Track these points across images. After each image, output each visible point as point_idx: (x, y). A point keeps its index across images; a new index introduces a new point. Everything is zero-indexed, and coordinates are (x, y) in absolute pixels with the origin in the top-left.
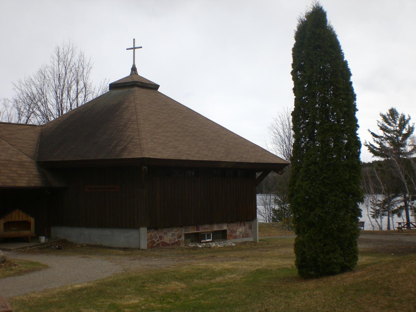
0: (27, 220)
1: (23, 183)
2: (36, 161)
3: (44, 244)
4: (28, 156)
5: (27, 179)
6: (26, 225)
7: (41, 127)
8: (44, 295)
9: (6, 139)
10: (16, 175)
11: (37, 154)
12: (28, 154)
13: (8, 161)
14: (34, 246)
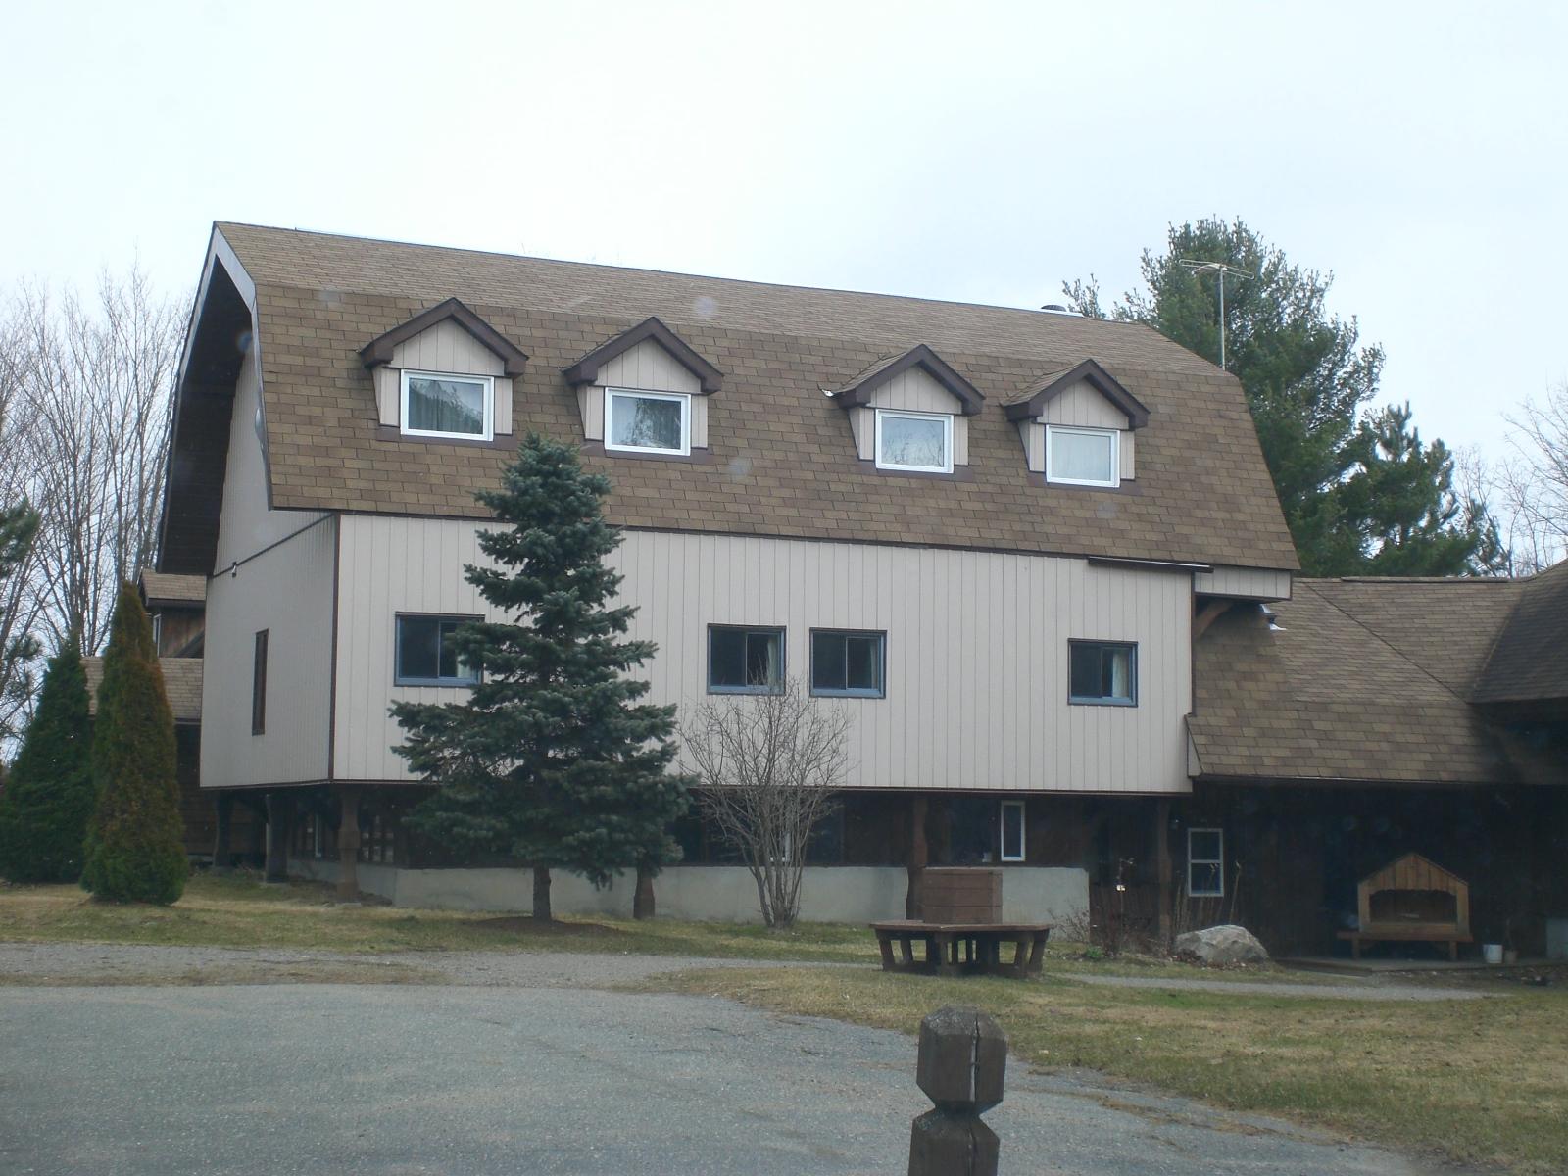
0: (1445, 889)
1: (1408, 769)
2: (1469, 703)
3: (1495, 968)
4: (1445, 687)
5: (1427, 757)
6: (1439, 903)
7: (1524, 585)
8: (1532, 1148)
9: (1386, 634)
10: (1384, 746)
11: (1478, 679)
12: (1449, 680)
13: (1363, 704)
14: (1476, 969)
